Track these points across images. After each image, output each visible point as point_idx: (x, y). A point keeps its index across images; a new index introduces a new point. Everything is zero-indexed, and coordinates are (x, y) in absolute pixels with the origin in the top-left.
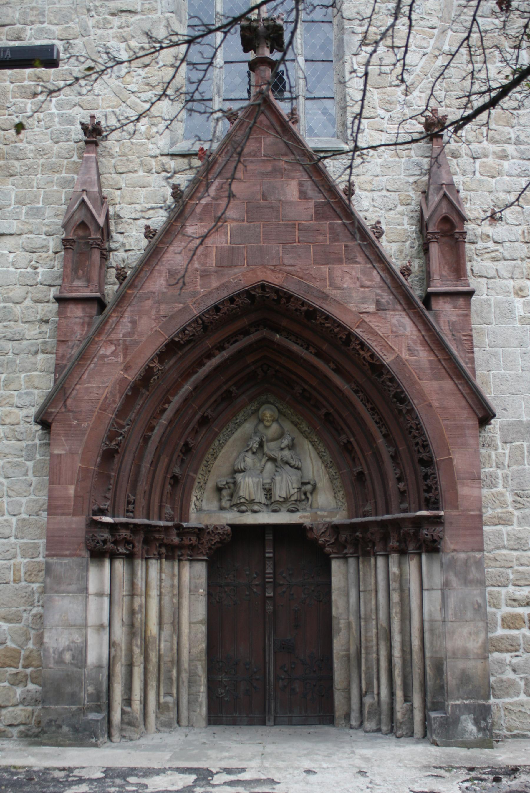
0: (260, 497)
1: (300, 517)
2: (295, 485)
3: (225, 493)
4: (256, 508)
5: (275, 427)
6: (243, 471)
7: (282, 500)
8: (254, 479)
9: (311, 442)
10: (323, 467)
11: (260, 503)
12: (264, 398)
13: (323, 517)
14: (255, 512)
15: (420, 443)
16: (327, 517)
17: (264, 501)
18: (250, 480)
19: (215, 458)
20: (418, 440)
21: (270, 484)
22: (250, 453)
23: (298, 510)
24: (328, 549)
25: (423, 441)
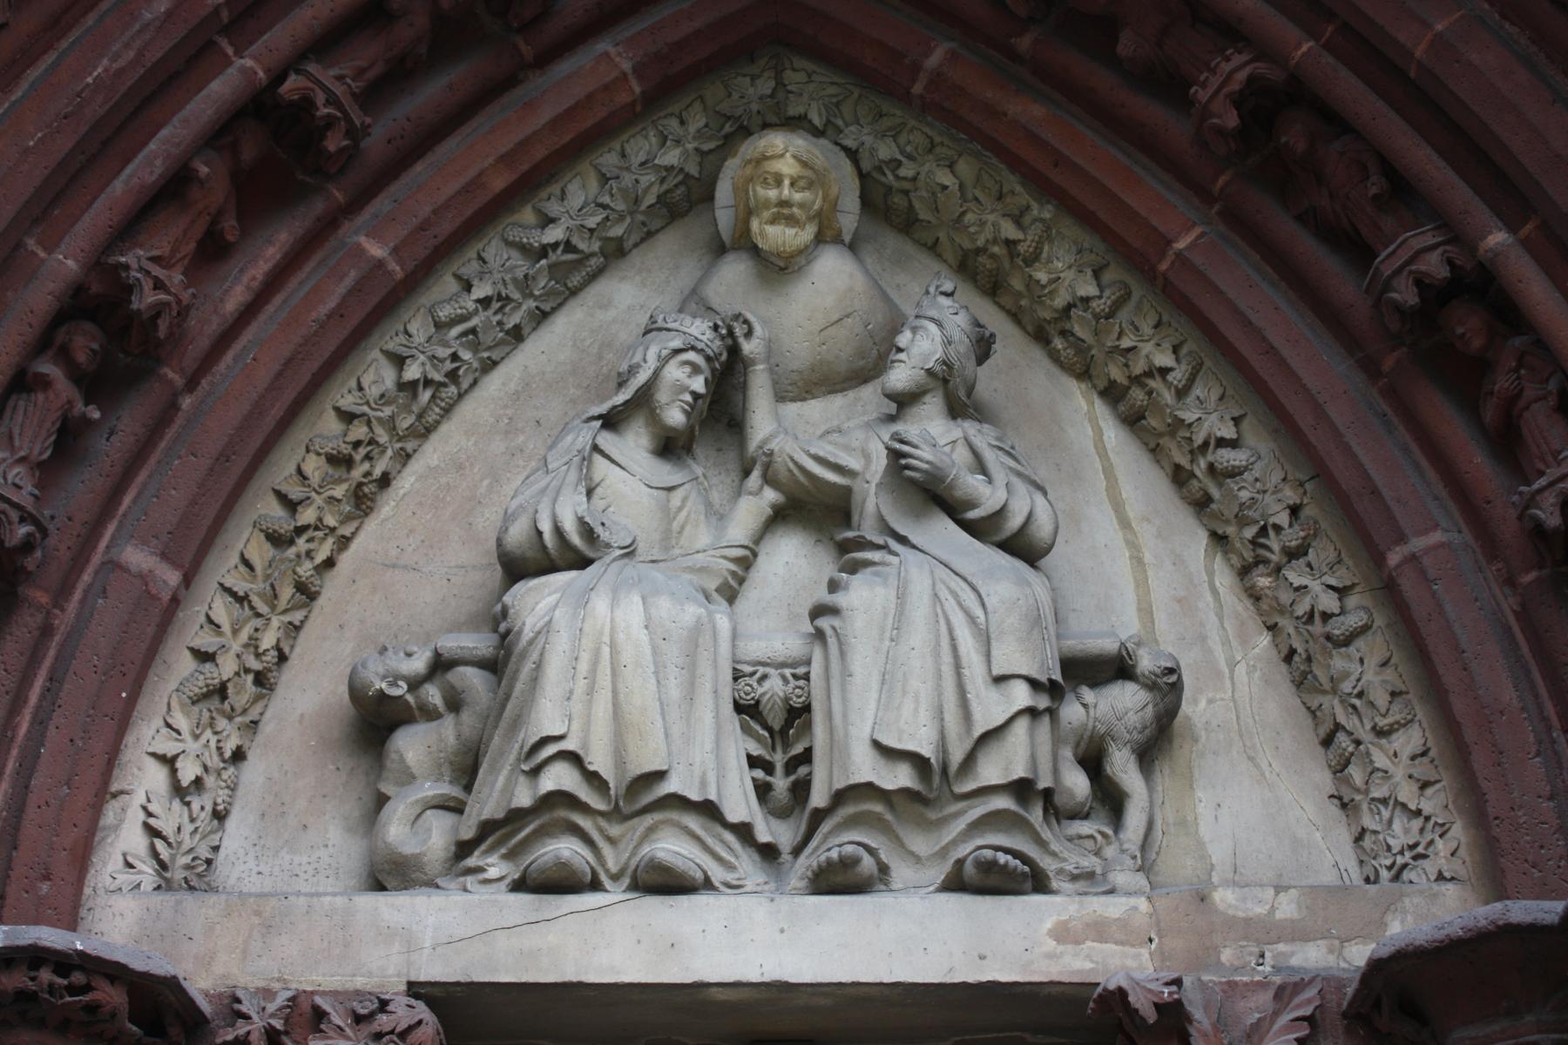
0: (711, 759)
1: (1062, 934)
2: (1013, 656)
3: (413, 746)
4: (673, 847)
5: (833, 279)
6: (582, 563)
7: (900, 777)
8: (664, 607)
9: (1112, 394)
10: (1224, 579)
11: (709, 810)
12: (752, 88)
14: (665, 883)
16: (1298, 933)
17: (740, 804)
18: (631, 612)
19: (362, 502)
21: (799, 671)
22: (633, 445)
23: (1038, 883)
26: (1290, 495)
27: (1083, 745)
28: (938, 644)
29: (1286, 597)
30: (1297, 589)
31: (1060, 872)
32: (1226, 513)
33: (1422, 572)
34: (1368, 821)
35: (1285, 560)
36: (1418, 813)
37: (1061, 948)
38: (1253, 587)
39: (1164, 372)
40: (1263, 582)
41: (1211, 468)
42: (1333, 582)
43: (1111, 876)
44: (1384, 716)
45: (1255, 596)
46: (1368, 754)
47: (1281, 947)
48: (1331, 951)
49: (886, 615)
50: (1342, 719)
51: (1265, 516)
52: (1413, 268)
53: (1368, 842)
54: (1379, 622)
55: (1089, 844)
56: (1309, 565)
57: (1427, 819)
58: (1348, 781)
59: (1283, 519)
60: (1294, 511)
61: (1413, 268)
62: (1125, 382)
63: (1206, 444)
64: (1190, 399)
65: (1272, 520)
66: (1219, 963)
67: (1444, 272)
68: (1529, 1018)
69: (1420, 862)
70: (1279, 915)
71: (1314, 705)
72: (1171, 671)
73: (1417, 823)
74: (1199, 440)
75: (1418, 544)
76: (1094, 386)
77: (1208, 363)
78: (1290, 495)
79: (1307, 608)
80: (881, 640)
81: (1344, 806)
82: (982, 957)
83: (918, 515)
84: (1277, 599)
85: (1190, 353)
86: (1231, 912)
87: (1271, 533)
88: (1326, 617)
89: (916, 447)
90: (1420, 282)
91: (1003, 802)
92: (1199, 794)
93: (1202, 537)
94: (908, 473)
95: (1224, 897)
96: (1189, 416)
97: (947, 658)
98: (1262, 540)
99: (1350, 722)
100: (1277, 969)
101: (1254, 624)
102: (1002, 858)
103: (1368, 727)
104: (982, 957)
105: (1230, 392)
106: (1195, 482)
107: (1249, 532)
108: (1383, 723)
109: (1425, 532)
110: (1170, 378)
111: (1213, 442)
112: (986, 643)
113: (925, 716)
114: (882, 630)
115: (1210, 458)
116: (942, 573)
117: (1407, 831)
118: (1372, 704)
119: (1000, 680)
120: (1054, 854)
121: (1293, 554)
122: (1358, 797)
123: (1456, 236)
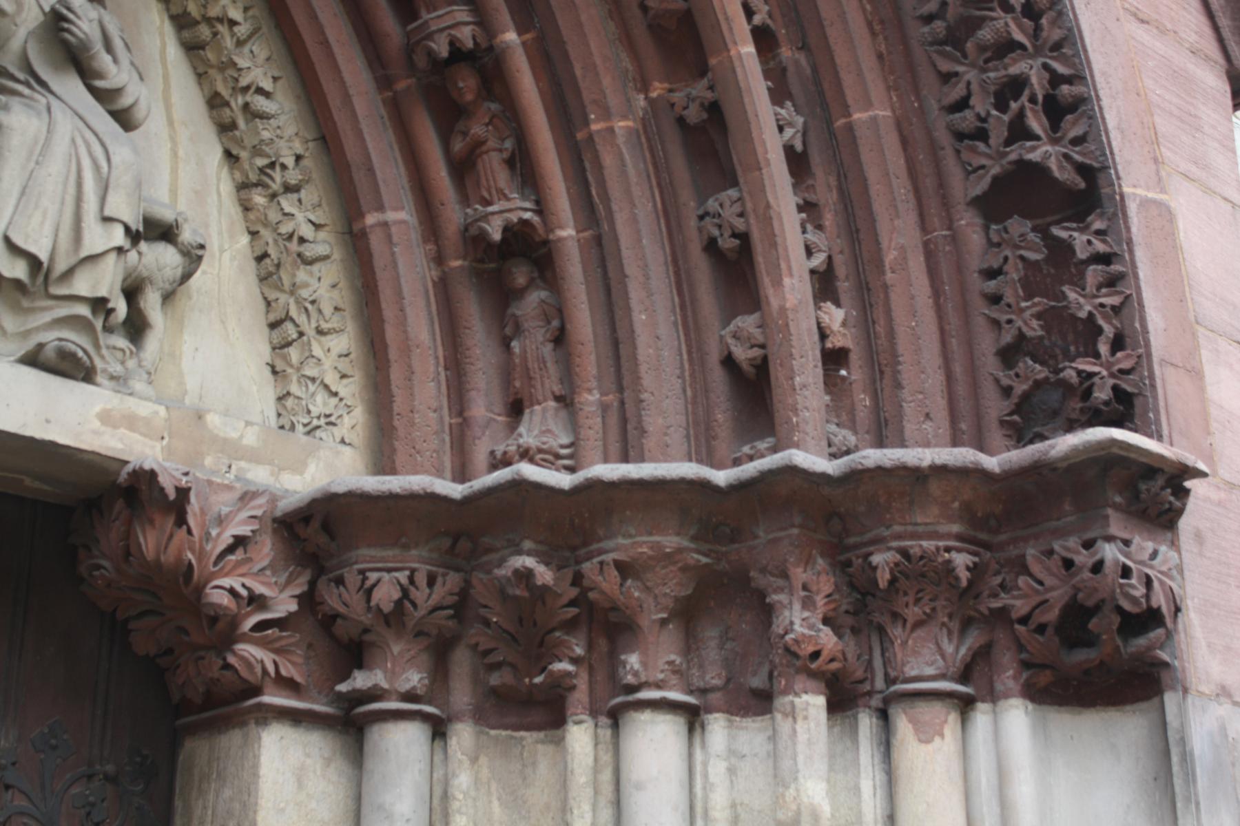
1: (106, 417)
10: (226, 187)
13: (233, 450)
15: (1038, 82)
16: (254, 457)
20: (1031, 69)
24: (253, 654)
25: (1056, 80)
26: (298, 147)
27: (129, 281)
28: (67, 178)
29: (274, 216)
30: (286, 214)
31: (104, 371)
32: (246, 141)
33: (389, 237)
34: (294, 389)
35: (282, 190)
36: (336, 394)
37: (103, 428)
38: (249, 200)
39: (233, 23)
40: (259, 199)
41: (246, 106)
42: (313, 218)
43: (131, 383)
44: (326, 321)
45: (246, 208)
46: (309, 342)
47: (243, 464)
48: (272, 474)
49: (36, 142)
50: (294, 313)
51: (279, 156)
52: (453, 32)
53: (290, 402)
54: (337, 255)
55: (119, 355)
56: (300, 201)
57: (341, 400)
58: (286, 359)
59: (290, 161)
60: (298, 158)
61: (453, 32)
62: (198, 18)
63: (247, 88)
64: (246, 49)
65: (282, 160)
66: (203, 465)
67: (470, 44)
68: (414, 552)
69: (330, 427)
70: (245, 442)
71: (272, 296)
72: (202, 247)
73: (334, 401)
74: (244, 82)
75: (391, 216)
76: (168, 10)
77: (264, 29)
78: (298, 147)
79: (290, 230)
80: (28, 159)
81: (274, 372)
82: (48, 421)
83: (57, 68)
84: (266, 215)
85: (253, 17)
86: (216, 431)
87: (278, 168)
88: (302, 240)
89: (79, 17)
90: (452, 43)
91: (84, 310)
92: (186, 337)
93: (218, 153)
94: (67, 36)
95: (213, 420)
96: (242, 63)
97: (72, 190)
98: (268, 171)
99: (301, 319)
100: (238, 478)
101: (240, 226)
102: (80, 354)
103: (314, 325)
104: (48, 421)
105: (275, 57)
106: (227, 111)
107: (261, 162)
108: (325, 326)
109: (396, 209)
110: (236, 29)
111: (253, 89)
112: (104, 190)
113: (48, 230)
114: (31, 153)
115: (248, 98)
116: (81, 124)
117: (325, 404)
118: (320, 311)
119: (107, 220)
120: (102, 357)
121: (289, 189)
122: (290, 370)
123: (483, 21)
